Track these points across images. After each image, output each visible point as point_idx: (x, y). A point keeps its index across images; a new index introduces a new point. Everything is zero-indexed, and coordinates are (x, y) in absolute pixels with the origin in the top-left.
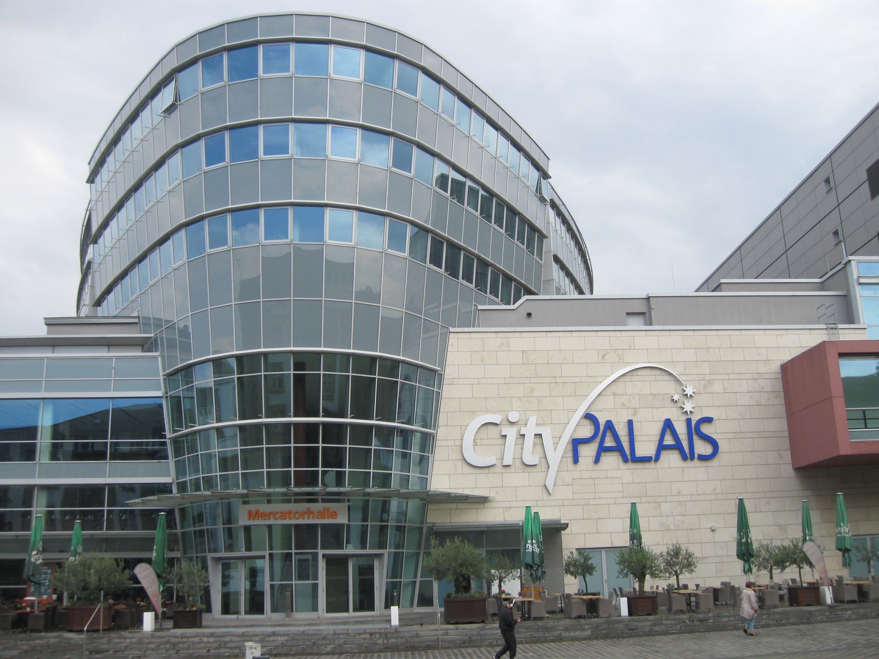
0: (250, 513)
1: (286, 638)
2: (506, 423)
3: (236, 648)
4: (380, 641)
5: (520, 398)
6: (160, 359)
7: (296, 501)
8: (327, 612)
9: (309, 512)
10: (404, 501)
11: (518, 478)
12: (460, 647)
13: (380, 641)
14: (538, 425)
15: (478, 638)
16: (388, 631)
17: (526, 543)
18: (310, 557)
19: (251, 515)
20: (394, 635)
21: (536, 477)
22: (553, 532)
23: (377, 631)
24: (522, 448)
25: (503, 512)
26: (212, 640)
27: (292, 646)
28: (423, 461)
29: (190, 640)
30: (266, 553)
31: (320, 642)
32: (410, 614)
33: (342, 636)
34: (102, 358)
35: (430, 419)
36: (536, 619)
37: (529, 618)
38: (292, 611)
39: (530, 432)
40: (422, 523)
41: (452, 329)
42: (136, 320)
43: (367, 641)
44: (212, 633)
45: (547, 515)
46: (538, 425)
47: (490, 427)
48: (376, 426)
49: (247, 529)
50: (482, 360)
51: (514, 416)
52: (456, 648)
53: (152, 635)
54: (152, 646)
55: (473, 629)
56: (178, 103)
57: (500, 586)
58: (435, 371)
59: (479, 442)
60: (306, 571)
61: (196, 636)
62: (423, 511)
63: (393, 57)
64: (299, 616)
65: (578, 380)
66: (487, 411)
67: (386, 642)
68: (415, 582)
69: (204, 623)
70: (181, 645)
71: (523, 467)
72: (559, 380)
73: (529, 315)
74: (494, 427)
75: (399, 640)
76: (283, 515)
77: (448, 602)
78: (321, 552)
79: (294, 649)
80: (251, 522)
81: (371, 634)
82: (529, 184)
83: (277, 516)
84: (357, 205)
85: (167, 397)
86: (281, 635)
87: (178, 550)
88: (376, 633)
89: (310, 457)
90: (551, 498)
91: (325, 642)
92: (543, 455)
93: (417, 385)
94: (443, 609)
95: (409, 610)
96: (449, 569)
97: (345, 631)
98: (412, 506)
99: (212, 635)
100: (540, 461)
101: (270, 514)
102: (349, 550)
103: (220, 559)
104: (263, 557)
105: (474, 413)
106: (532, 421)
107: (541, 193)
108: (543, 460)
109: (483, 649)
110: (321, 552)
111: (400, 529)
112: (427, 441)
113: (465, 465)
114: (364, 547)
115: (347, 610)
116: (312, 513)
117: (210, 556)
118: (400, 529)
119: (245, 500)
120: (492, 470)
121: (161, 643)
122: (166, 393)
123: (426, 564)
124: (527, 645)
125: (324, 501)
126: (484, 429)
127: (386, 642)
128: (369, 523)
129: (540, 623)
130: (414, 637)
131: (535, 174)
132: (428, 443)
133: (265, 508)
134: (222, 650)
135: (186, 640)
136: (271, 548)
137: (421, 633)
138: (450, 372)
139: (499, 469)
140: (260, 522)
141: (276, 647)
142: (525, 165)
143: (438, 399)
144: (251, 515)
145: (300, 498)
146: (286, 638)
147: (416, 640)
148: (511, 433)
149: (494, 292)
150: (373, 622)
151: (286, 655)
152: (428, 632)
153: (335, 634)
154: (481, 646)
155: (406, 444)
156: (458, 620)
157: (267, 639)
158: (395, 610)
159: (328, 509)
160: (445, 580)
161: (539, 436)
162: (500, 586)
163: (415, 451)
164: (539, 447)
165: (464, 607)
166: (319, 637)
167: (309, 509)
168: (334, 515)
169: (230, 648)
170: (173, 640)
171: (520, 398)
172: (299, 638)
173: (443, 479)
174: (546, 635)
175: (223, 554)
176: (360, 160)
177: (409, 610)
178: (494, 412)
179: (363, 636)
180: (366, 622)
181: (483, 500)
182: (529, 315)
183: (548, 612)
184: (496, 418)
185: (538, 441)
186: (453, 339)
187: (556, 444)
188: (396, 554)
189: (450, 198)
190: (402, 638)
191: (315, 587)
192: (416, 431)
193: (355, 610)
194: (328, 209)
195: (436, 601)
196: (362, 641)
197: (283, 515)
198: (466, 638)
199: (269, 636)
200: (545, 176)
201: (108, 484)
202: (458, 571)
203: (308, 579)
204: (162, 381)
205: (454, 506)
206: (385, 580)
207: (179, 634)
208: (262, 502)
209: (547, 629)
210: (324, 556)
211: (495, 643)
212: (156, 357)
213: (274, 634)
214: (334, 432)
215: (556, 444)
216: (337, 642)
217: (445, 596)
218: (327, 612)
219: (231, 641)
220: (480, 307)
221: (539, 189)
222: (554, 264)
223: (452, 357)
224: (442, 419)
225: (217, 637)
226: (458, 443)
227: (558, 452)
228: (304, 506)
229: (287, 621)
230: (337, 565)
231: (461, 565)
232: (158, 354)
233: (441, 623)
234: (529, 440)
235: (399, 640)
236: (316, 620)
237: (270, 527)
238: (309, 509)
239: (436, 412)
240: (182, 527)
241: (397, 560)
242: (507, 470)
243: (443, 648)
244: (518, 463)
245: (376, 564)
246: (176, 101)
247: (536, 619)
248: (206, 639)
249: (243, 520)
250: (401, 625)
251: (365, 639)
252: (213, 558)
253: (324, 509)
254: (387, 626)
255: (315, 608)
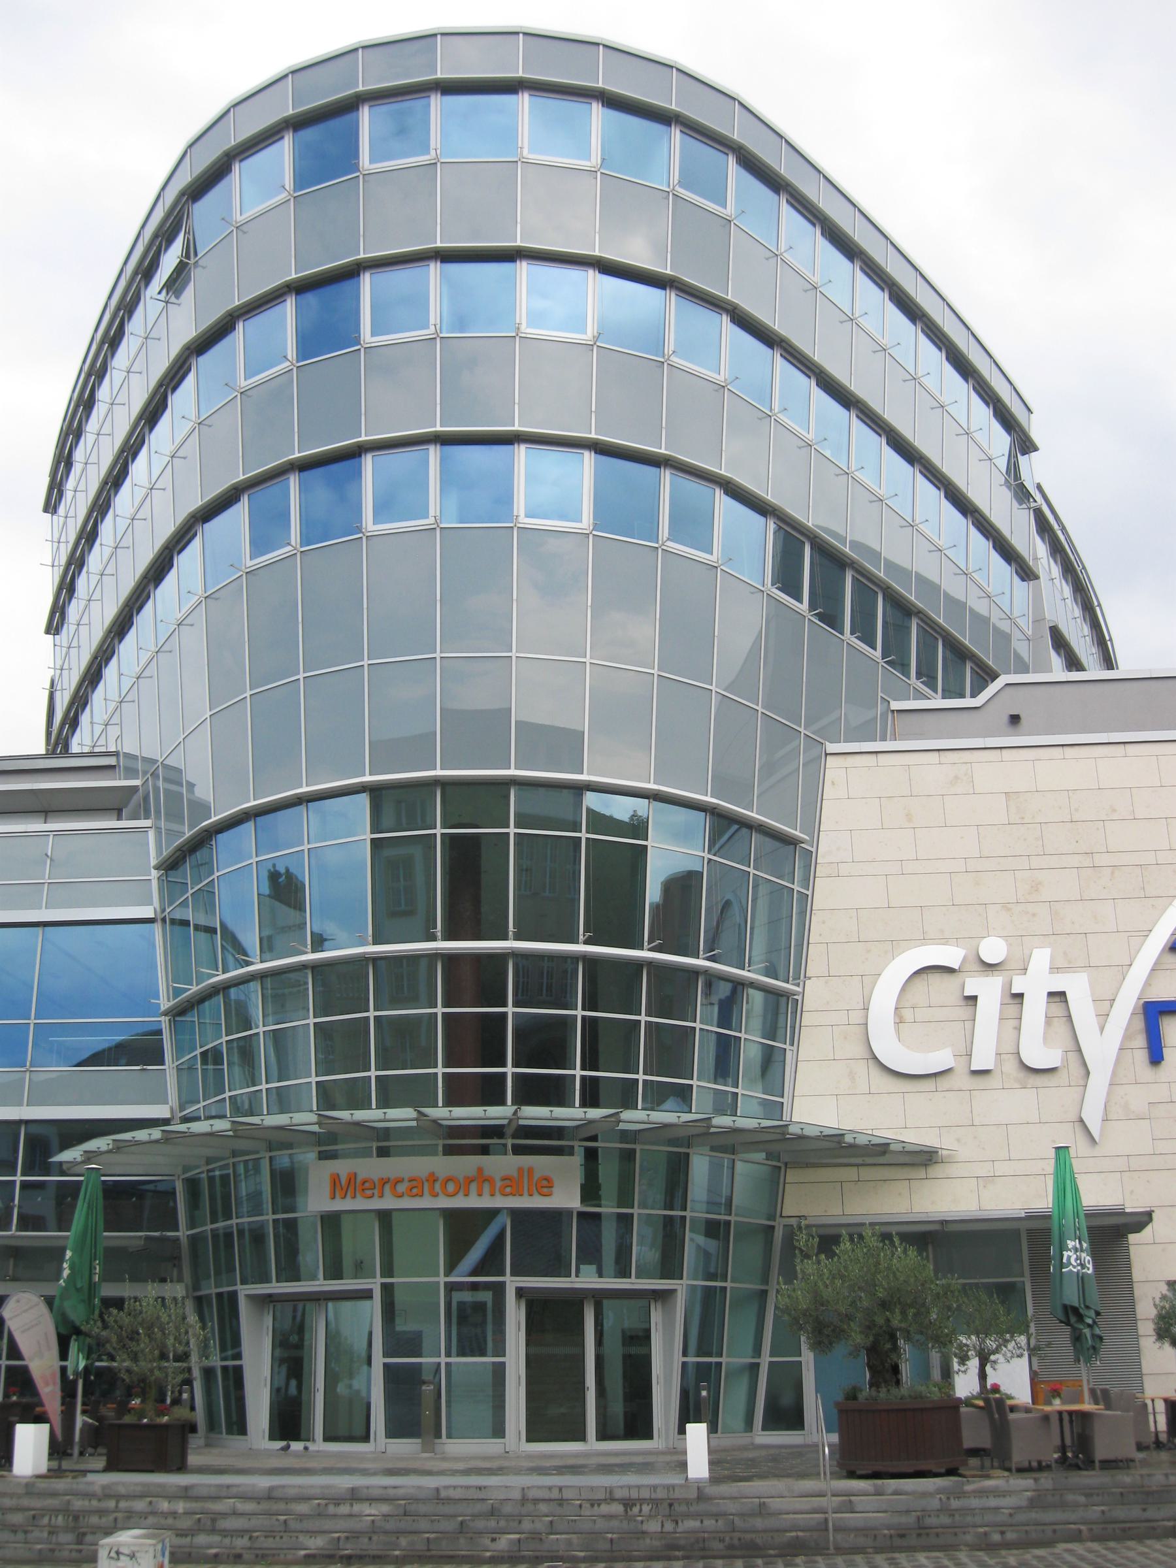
0: (335, 1180)
1: (385, 1508)
2: (976, 967)
3: (241, 1533)
4: (653, 1526)
5: (1006, 906)
6: (151, 835)
7: (450, 1151)
8: (528, 1440)
9: (481, 1179)
10: (726, 1157)
11: (1010, 1103)
12: (893, 1549)
13: (653, 1526)
14: (1055, 969)
15: (945, 1520)
16: (677, 1494)
17: (1062, 1247)
18: (486, 1297)
19: (337, 1187)
20: (694, 1508)
21: (1055, 1098)
22: (1112, 1233)
23: (645, 1494)
24: (1018, 1029)
25: (989, 1178)
26: (181, 1506)
27: (399, 1533)
28: (771, 1064)
29: (123, 1504)
30: (375, 1284)
31: (480, 1524)
32: (745, 1448)
33: (543, 1508)
34: (25, 834)
35: (787, 954)
36: (1109, 1465)
37: (1089, 1463)
38: (438, 1435)
39: (1035, 984)
40: (772, 1217)
41: (831, 747)
42: (111, 761)
43: (615, 1523)
44: (186, 1488)
45: (1098, 1193)
46: (1055, 969)
47: (935, 979)
48: (650, 964)
49: (331, 1222)
50: (909, 817)
51: (993, 949)
52: (879, 1550)
53: (30, 1487)
54: (17, 1518)
55: (924, 1495)
56: (192, 261)
57: (983, 1376)
58: (790, 842)
59: (908, 1014)
60: (475, 1327)
61: (141, 1496)
62: (773, 1186)
63: (663, 117)
64: (457, 1448)
65: (1150, 858)
66: (925, 940)
67: (669, 1526)
68: (754, 1368)
69: (193, 1459)
70: (94, 1520)
71: (1022, 1074)
72: (1100, 860)
73: (1015, 719)
74: (946, 977)
75: (709, 1523)
76: (416, 1186)
77: (850, 1416)
78: (512, 1283)
79: (403, 1542)
80: (339, 1205)
81: (628, 1504)
82: (993, 453)
83: (401, 1188)
84: (652, 786)
85: (164, 920)
86: (371, 1500)
87: (180, 1279)
88: (642, 1501)
89: (484, 1040)
90: (1097, 1151)
91: (492, 1524)
92: (1070, 1045)
93: (751, 870)
94: (835, 1438)
95: (741, 1439)
96: (849, 1317)
97: (555, 1494)
98: (747, 1169)
99: (185, 1493)
100: (1065, 1060)
101: (384, 1182)
102: (586, 1279)
103: (270, 1299)
104: (367, 1295)
105: (895, 946)
106: (1041, 958)
107: (1017, 476)
108: (1072, 1057)
109: (963, 1556)
110: (512, 1283)
111: (714, 1229)
112: (781, 1010)
113: (875, 1072)
114: (624, 1273)
115: (581, 1437)
116: (490, 1180)
117: (244, 1291)
118: (714, 1229)
119: (329, 1143)
120: (943, 1083)
121: (45, 1511)
122: (163, 910)
123: (784, 1301)
124: (1095, 1546)
125: (518, 1150)
126: (920, 984)
127: (669, 1526)
128: (635, 1211)
129: (1126, 1478)
130: (752, 1515)
131: (1001, 441)
132: (781, 1023)
133: (372, 1168)
134: (201, 1539)
135: (111, 1504)
136: (388, 1271)
137: (775, 1504)
138: (831, 846)
139: (961, 1080)
140: (360, 1204)
141: (354, 1535)
142: (982, 413)
143: (803, 913)
144: (337, 1187)
145: (458, 1141)
146: (385, 1508)
147: (759, 1523)
148: (988, 990)
149: (927, 675)
150: (646, 1468)
151: (376, 1559)
152: (793, 1499)
153: (524, 1500)
154: (954, 1547)
155: (727, 1013)
156: (879, 1467)
157: (332, 1509)
158: (697, 1433)
159: (531, 1171)
160: (840, 1350)
161: (1058, 996)
162: (983, 1376)
163: (750, 1039)
164: (1060, 1027)
165: (899, 1433)
166: (479, 1508)
167: (480, 1170)
168: (546, 1185)
169: (225, 1533)
170: (78, 1504)
171: (1006, 906)
172: (423, 1508)
173: (822, 1096)
174: (1151, 1513)
175: (276, 1287)
176: (596, 338)
177: (741, 1439)
178: (945, 941)
179: (605, 1509)
180: (624, 1468)
181: (924, 1159)
182: (1015, 719)
183: (1140, 1447)
184: (950, 956)
185: (1057, 1009)
186: (834, 769)
187: (1103, 1018)
188: (709, 1293)
189: (808, 615)
190: (716, 1516)
191: (499, 1372)
192: (753, 985)
193: (604, 1435)
194: (523, 447)
195: (813, 1406)
196: (601, 1525)
197: (416, 1186)
198: (911, 1519)
199: (338, 1501)
200: (1024, 444)
201: (27, 1122)
202: (880, 1320)
203: (483, 1354)
204: (155, 884)
205: (850, 1173)
206: (678, 1359)
207: (97, 1489)
208: (365, 1153)
209: (1149, 1496)
210: (520, 1292)
211: (996, 1537)
212: (144, 830)
213: (354, 1496)
214: (546, 980)
215: (1103, 1018)
216: (527, 1525)
217: (840, 1398)
218: (528, 1440)
219: (235, 1513)
220: (895, 705)
221: (1013, 470)
222: (1053, 653)
223: (832, 813)
224: (816, 960)
225: (197, 1499)
226: (856, 1017)
227: (1107, 1038)
228: (468, 1164)
229: (426, 1460)
230: (552, 1318)
231: (884, 1305)
232: (147, 823)
233: (835, 1476)
234: (1035, 1008)
235: (709, 1523)
236: (496, 1460)
237: (385, 1217)
238: (480, 1170)
239: (800, 945)
240: (192, 1224)
241: (709, 1305)
242: (980, 1082)
243: (840, 1551)
244: (1010, 1066)
245: (656, 1316)
246: (188, 256)
247: (1109, 1465)
248: (165, 1506)
249: (317, 1200)
250: (714, 1479)
251: (610, 1517)
252: (251, 1298)
253: (520, 1170)
254: (674, 1479)
255: (499, 1431)
